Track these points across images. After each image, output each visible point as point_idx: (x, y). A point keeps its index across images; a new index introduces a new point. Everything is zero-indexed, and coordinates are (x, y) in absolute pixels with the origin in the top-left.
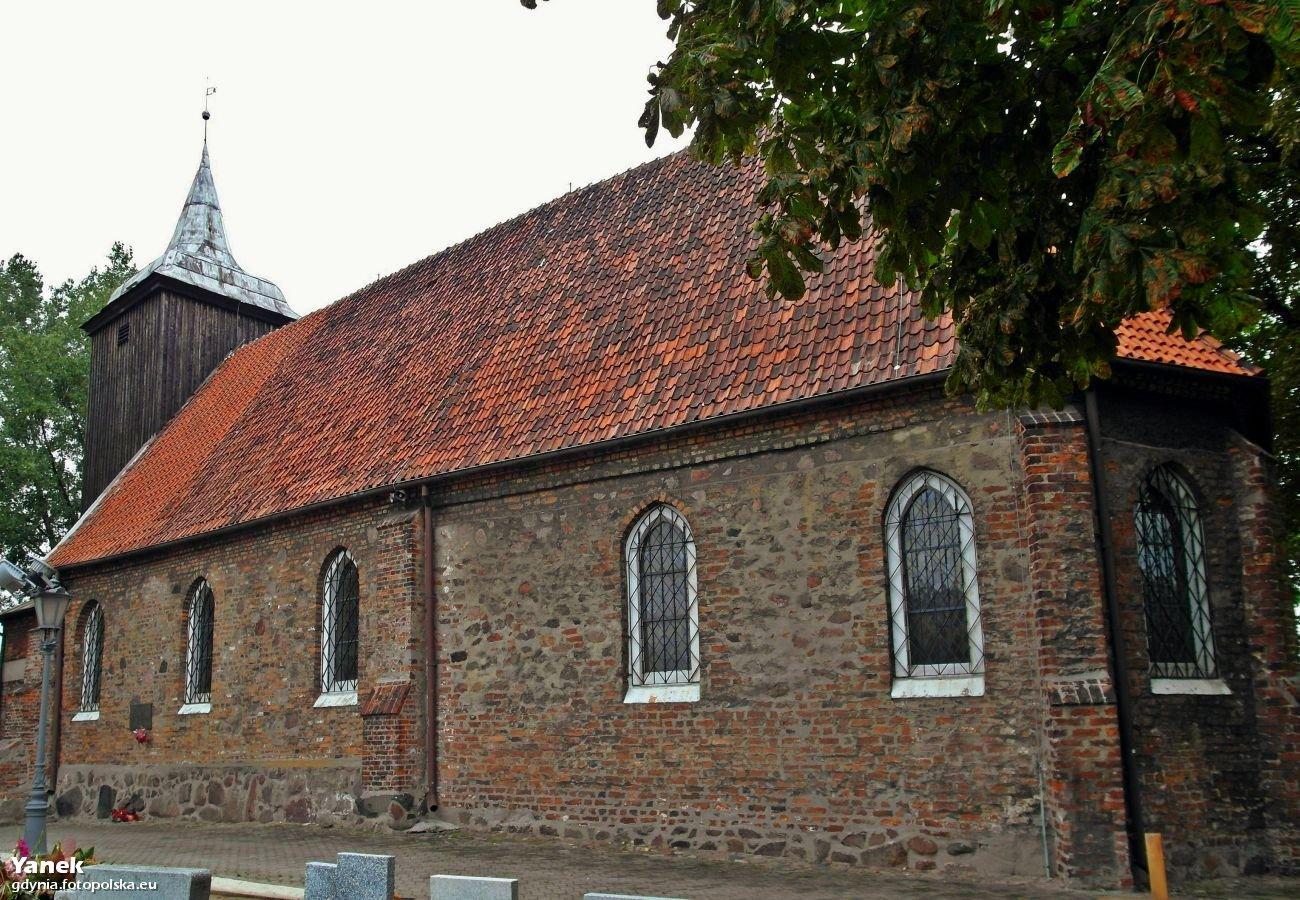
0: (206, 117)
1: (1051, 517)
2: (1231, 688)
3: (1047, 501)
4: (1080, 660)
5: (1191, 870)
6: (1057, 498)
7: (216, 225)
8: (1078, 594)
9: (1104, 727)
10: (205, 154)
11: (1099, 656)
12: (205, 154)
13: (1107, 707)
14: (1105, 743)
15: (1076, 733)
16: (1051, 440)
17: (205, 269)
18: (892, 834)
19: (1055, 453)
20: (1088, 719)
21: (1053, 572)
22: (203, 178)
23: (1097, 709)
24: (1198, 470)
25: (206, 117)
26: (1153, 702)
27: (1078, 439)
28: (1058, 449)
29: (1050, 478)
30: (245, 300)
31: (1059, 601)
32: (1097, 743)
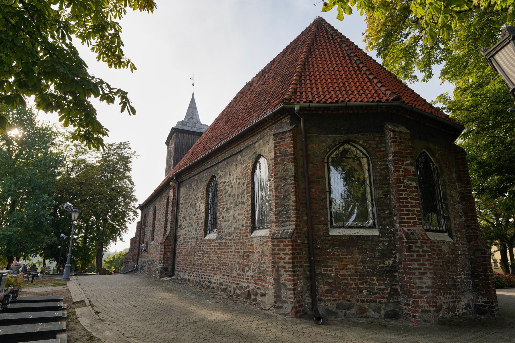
0: (193, 85)
1: (279, 167)
2: (380, 233)
3: (278, 161)
4: (287, 221)
5: (348, 312)
6: (282, 160)
7: (194, 113)
8: (287, 195)
9: (287, 248)
10: (193, 94)
11: (292, 219)
12: (193, 94)
13: (288, 239)
14: (287, 254)
15: (278, 250)
16: (281, 139)
17: (188, 125)
18: (249, 287)
19: (282, 143)
20: (282, 244)
21: (279, 188)
22: (193, 101)
23: (285, 240)
24: (364, 141)
25: (193, 85)
26: (330, 238)
27: (290, 137)
28: (283, 141)
29: (280, 153)
30: (198, 131)
31: (281, 198)
32: (284, 254)
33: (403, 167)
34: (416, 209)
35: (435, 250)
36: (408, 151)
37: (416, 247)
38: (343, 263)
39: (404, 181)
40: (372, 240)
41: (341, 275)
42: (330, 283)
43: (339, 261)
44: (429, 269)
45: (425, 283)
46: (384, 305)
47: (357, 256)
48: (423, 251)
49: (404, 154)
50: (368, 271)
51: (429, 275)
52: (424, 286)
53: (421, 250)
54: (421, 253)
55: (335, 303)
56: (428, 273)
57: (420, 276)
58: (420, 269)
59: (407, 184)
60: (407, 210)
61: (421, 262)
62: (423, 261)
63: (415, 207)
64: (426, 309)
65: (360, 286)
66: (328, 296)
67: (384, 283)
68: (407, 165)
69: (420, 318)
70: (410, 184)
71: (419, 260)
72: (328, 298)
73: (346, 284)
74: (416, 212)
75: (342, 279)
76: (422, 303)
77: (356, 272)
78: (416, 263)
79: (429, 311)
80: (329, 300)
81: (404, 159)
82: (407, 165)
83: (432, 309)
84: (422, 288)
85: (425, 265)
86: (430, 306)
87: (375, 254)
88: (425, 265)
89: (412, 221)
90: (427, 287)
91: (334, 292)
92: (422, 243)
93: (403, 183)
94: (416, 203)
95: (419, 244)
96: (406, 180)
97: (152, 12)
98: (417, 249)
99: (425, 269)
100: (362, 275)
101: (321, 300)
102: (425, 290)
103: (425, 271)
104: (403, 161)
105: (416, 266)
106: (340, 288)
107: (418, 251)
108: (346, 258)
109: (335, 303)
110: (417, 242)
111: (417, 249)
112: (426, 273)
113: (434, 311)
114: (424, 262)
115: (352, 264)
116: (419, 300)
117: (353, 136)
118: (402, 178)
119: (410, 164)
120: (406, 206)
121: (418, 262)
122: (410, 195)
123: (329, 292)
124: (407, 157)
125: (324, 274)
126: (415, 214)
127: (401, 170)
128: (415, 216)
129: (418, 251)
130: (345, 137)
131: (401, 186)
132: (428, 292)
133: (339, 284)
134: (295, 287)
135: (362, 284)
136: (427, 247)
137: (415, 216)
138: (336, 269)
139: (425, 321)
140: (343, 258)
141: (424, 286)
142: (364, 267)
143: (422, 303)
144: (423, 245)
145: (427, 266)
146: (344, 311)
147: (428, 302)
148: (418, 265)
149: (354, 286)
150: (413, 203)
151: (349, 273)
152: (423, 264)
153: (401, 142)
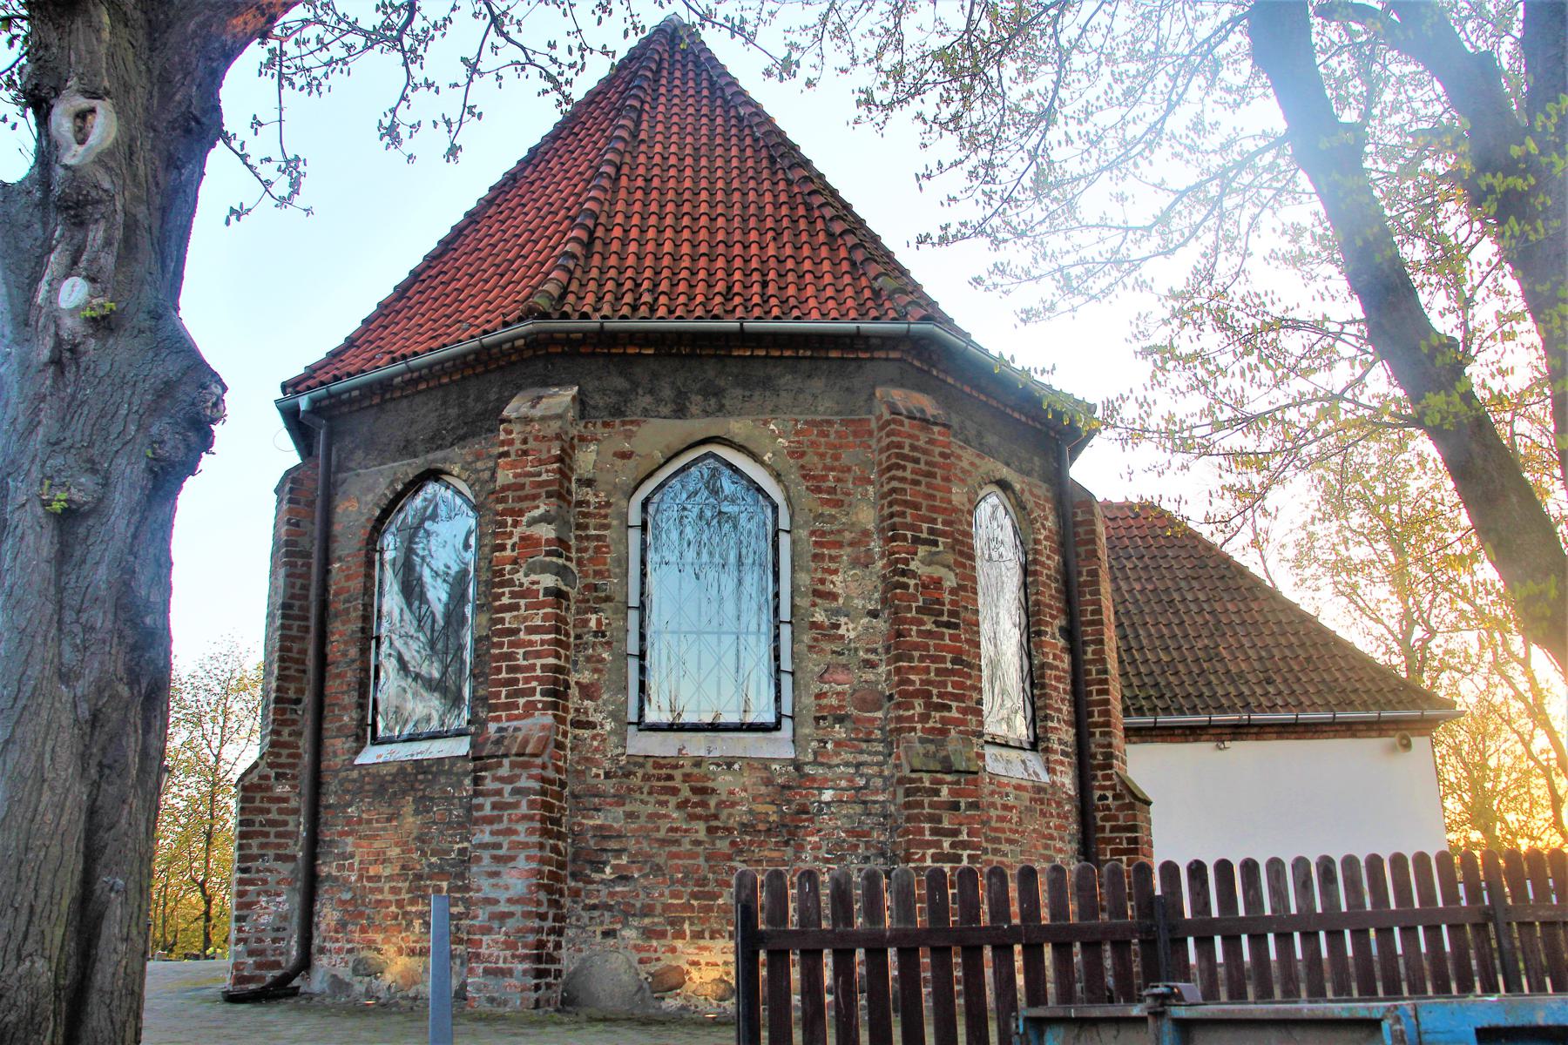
26: (355, 774)
33: (519, 529)
34: (539, 662)
35: (674, 791)
36: (544, 477)
37: (496, 779)
38: (377, 845)
39: (515, 577)
40: (449, 773)
41: (370, 879)
42: (344, 902)
43: (367, 837)
44: (526, 845)
45: (507, 888)
46: (458, 961)
47: (411, 821)
48: (516, 791)
49: (528, 491)
50: (430, 865)
51: (521, 863)
52: (503, 896)
53: (508, 788)
54: (507, 798)
55: (351, 958)
56: (522, 856)
57: (494, 869)
58: (498, 846)
59: (521, 585)
60: (510, 669)
61: (504, 825)
62: (510, 820)
63: (538, 655)
64: (501, 964)
65: (408, 908)
66: (337, 940)
67: (462, 899)
68: (534, 522)
69: (479, 990)
70: (533, 583)
71: (500, 819)
72: (337, 945)
73: (379, 902)
74: (538, 672)
75: (372, 890)
76: (489, 947)
77: (403, 867)
78: (487, 828)
79: (509, 973)
80: (340, 950)
81: (525, 505)
82: (534, 522)
83: (520, 967)
84: (496, 902)
85: (515, 832)
86: (513, 956)
87: (451, 812)
88: (515, 832)
89: (522, 701)
90: (509, 901)
91: (350, 927)
92: (513, 765)
93: (511, 583)
94: (543, 642)
95: (504, 771)
96: (521, 574)
97: (387, 147)
98: (497, 785)
99: (515, 846)
100: (419, 877)
101: (322, 950)
102: (503, 907)
103: (512, 853)
104: (521, 513)
105: (487, 838)
106: (361, 915)
107: (499, 792)
108: (384, 829)
109: (351, 958)
110: (500, 765)
111: (497, 785)
112: (513, 858)
113: (525, 972)
114: (515, 826)
115: (397, 844)
116: (485, 938)
117: (439, 454)
118: (508, 567)
119: (545, 519)
120: (510, 657)
121: (496, 827)
122: (525, 619)
123: (342, 926)
124: (535, 497)
125: (336, 878)
126: (537, 678)
127: (509, 543)
128: (534, 684)
129: (499, 792)
130: (409, 468)
131: (503, 594)
132: (511, 915)
133: (363, 904)
134: (244, 912)
135: (413, 902)
136: (530, 777)
137: (534, 684)
138: (361, 862)
139: (491, 1000)
140: (378, 829)
141: (503, 896)
142: (423, 853)
143: (489, 947)
144: (517, 771)
145: (522, 838)
146: (367, 979)
147: (509, 945)
148: (492, 833)
149: (393, 908)
150: (531, 643)
151: (387, 872)
152: (509, 832)
153: (525, 453)
